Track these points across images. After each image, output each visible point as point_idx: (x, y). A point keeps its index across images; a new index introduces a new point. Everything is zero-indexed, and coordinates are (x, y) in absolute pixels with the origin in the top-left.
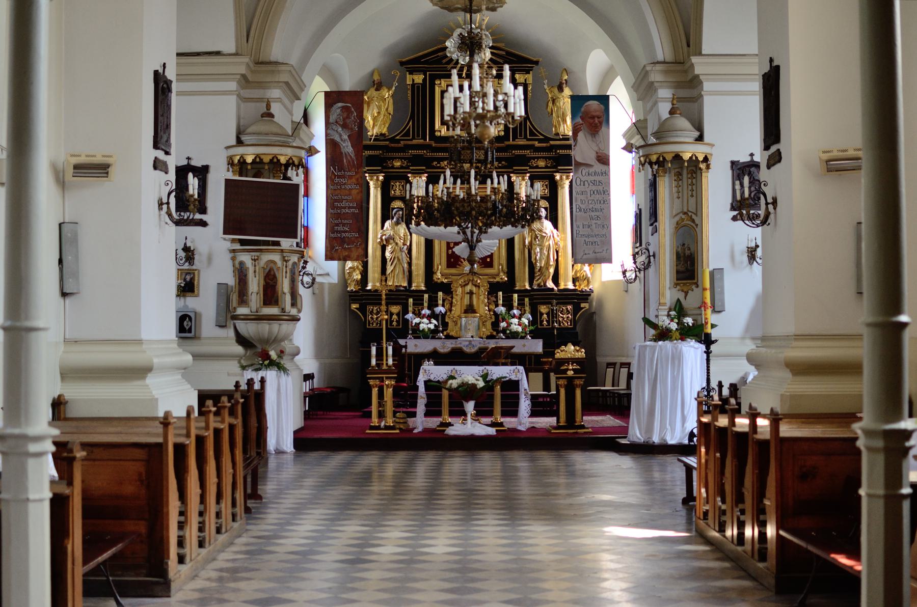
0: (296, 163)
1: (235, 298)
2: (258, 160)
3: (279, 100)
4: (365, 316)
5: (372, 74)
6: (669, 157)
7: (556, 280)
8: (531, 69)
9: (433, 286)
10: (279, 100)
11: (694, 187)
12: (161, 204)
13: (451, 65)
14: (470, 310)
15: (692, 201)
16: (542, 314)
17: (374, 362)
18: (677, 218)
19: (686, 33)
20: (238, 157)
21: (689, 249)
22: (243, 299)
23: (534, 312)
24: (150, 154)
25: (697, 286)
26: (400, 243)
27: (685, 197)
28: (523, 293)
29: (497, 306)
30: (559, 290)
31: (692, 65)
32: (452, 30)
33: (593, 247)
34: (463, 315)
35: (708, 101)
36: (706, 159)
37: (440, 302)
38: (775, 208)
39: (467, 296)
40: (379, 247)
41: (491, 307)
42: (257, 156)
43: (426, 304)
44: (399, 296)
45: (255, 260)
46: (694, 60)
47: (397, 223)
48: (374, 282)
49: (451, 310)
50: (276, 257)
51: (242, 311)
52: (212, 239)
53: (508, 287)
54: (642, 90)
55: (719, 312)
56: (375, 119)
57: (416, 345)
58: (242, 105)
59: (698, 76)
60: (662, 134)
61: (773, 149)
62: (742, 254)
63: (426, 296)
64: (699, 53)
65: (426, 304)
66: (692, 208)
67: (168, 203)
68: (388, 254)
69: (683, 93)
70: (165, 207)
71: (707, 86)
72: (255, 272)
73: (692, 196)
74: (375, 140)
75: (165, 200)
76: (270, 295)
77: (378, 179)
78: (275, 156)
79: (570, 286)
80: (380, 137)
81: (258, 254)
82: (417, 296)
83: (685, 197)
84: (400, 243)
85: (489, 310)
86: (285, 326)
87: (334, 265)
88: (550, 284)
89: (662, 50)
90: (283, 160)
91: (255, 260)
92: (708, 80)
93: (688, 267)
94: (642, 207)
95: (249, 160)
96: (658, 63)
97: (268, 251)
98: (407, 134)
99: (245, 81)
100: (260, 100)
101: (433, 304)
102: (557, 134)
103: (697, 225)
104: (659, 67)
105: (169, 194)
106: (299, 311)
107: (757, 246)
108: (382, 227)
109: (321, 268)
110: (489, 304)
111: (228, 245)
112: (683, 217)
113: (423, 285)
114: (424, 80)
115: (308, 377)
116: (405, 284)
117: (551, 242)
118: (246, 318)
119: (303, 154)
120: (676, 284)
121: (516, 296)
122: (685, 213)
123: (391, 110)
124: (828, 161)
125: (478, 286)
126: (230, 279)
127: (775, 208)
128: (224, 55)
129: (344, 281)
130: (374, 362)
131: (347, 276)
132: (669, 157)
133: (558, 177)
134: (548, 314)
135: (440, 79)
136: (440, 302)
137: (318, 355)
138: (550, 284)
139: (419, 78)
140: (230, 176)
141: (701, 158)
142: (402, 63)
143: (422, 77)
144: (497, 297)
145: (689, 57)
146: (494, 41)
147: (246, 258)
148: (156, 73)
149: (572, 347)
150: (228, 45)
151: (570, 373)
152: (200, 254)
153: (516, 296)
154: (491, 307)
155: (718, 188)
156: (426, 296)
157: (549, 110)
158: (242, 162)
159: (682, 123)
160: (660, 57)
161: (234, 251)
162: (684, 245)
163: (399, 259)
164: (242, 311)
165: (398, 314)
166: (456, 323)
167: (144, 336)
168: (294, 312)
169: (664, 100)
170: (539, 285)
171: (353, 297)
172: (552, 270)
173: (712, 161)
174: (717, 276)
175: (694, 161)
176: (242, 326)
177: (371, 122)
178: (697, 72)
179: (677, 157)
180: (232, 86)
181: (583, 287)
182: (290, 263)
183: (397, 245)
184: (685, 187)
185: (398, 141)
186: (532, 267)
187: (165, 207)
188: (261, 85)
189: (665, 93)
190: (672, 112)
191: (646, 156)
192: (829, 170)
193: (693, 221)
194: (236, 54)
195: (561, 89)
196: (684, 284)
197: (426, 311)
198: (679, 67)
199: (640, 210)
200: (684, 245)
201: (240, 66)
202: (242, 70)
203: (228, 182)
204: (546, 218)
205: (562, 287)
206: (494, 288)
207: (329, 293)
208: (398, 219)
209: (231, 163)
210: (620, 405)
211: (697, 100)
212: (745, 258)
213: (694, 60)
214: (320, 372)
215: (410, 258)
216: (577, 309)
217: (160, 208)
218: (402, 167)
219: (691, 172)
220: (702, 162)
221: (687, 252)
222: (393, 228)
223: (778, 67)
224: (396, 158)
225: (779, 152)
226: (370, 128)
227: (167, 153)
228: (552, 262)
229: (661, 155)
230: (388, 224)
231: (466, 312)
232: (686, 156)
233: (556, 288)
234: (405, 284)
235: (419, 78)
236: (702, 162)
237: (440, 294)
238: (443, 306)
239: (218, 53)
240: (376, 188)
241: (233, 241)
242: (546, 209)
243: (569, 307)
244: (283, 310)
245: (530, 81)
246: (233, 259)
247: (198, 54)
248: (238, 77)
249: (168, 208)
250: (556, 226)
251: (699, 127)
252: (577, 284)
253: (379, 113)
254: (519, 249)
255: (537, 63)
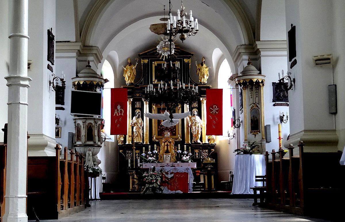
0: (100, 84)
1: (75, 138)
2: (85, 83)
3: (93, 61)
4: (125, 156)
5: (127, 59)
6: (248, 81)
7: (201, 139)
8: (190, 57)
9: (152, 143)
10: (93, 61)
11: (258, 93)
12: (50, 83)
13: (159, 56)
14: (167, 152)
15: (257, 98)
16: (196, 153)
17: (129, 165)
18: (251, 106)
19: (253, 31)
20: (77, 82)
21: (256, 118)
22: (79, 139)
23: (193, 152)
24: (47, 62)
25: (260, 132)
26: (139, 125)
27: (254, 97)
28: (188, 145)
29: (178, 150)
30: (202, 144)
31: (257, 44)
32: (159, 42)
33: (215, 126)
34: (164, 154)
35: (262, 59)
36: (262, 82)
37: (155, 149)
38: (294, 83)
39: (166, 147)
40: (131, 127)
41: (175, 150)
42: (85, 81)
43: (150, 150)
44: (139, 146)
45: (84, 123)
46: (257, 43)
47: (138, 117)
48: (129, 141)
49: (159, 152)
50: (92, 122)
51: (78, 143)
52: (67, 114)
53: (182, 143)
54: (236, 59)
55: (269, 142)
56: (129, 77)
57: (146, 166)
58: (78, 63)
59: (259, 49)
60: (245, 72)
61: (293, 60)
62: (278, 119)
63: (150, 146)
64: (259, 40)
65: (150, 150)
66: (257, 102)
67: (53, 83)
68: (134, 130)
69: (253, 57)
70: (52, 84)
71: (262, 53)
72: (84, 127)
73: (257, 97)
74: (129, 85)
75: (52, 82)
76: (90, 136)
77: (130, 100)
78: (92, 81)
79: (207, 142)
80: (131, 84)
81: (85, 120)
82: (146, 146)
83: (254, 97)
84: (139, 125)
85: (175, 152)
86: (96, 149)
87: (113, 137)
88: (199, 141)
89: (244, 40)
90: (95, 83)
91: (84, 123)
92: (263, 51)
93: (255, 124)
94: (236, 109)
95: (81, 83)
96: (242, 45)
97: (89, 119)
98: (142, 83)
99: (80, 54)
100: (85, 61)
101: (152, 149)
102: (201, 83)
103: (259, 108)
104: (243, 47)
105: (54, 79)
106: (101, 144)
107: (284, 116)
108: (132, 119)
109: (108, 136)
110: (175, 149)
111: (73, 117)
112: (254, 105)
113: (148, 142)
114: (148, 62)
115: (104, 178)
116: (142, 142)
117: (199, 125)
118: (80, 146)
119: (103, 81)
120: (251, 132)
121: (185, 146)
122: (254, 104)
123: (135, 73)
124: (316, 60)
125: (170, 143)
126: (74, 131)
127: (294, 83)
128: (71, 42)
129: (117, 141)
130: (129, 165)
131: (118, 139)
132: (248, 81)
133: (201, 99)
134: (198, 153)
135: (154, 61)
136: (155, 149)
137: (107, 170)
138: (199, 141)
139: (146, 61)
140: (74, 90)
141: (260, 81)
142: (139, 55)
143: (147, 60)
144: (178, 147)
145: (255, 42)
146: (176, 46)
147: (80, 122)
148: (48, 30)
149: (210, 159)
150: (73, 39)
151: (209, 169)
152: (61, 121)
153: (185, 146)
154: (175, 150)
155: (267, 93)
156: (150, 146)
157: (198, 73)
158: (79, 83)
159: (253, 68)
160: (244, 43)
161: (75, 119)
162: (254, 116)
163: (139, 131)
164: (78, 143)
165: (138, 154)
166: (161, 157)
167: (44, 133)
168: (99, 143)
169: (245, 60)
170: (194, 142)
171: (120, 147)
172: (200, 136)
173: (265, 83)
174: (268, 128)
175: (257, 83)
176: (78, 149)
177: (127, 78)
178: (258, 47)
179: (251, 81)
180: (74, 54)
181: (212, 142)
182: (98, 124)
183: (139, 125)
184: (254, 95)
185: (138, 86)
186: (192, 135)
187: (52, 84)
188: (86, 55)
189: (246, 57)
190: (249, 64)
191: (239, 81)
192: (317, 64)
193: (258, 107)
194: (76, 42)
195: (202, 65)
196: (255, 132)
197: (150, 152)
198: (251, 47)
199: (235, 110)
200: (254, 116)
201: (78, 46)
202: (79, 48)
203: (73, 92)
204: (197, 115)
205: (204, 142)
206: (176, 144)
207: (111, 146)
208: (138, 116)
209: (74, 84)
210: (229, 186)
211: (258, 59)
212: (279, 121)
213: (257, 43)
214: (107, 177)
215: (143, 131)
216: (210, 151)
217: (50, 85)
218: (139, 96)
219: (255, 87)
220: (261, 83)
221: (255, 119)
222: (136, 120)
223: (295, 27)
224: (137, 93)
225: (295, 60)
226: (127, 81)
227: (53, 64)
228: (200, 132)
229: (244, 80)
230: (134, 118)
231: (165, 152)
232: (255, 80)
233: (201, 143)
234: (142, 142)
235: (146, 61)
236: (261, 83)
237: (155, 145)
238: (156, 150)
239: (68, 42)
240: (129, 104)
241: (75, 115)
242: (197, 112)
243: (207, 151)
244: (95, 143)
245: (190, 62)
246: (75, 122)
247: (61, 42)
248: (77, 51)
249: (53, 84)
250: (201, 118)
251: (260, 70)
252: (210, 141)
253: (130, 75)
254: (186, 132)
255: (193, 55)
